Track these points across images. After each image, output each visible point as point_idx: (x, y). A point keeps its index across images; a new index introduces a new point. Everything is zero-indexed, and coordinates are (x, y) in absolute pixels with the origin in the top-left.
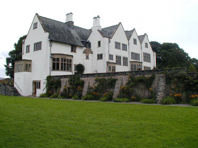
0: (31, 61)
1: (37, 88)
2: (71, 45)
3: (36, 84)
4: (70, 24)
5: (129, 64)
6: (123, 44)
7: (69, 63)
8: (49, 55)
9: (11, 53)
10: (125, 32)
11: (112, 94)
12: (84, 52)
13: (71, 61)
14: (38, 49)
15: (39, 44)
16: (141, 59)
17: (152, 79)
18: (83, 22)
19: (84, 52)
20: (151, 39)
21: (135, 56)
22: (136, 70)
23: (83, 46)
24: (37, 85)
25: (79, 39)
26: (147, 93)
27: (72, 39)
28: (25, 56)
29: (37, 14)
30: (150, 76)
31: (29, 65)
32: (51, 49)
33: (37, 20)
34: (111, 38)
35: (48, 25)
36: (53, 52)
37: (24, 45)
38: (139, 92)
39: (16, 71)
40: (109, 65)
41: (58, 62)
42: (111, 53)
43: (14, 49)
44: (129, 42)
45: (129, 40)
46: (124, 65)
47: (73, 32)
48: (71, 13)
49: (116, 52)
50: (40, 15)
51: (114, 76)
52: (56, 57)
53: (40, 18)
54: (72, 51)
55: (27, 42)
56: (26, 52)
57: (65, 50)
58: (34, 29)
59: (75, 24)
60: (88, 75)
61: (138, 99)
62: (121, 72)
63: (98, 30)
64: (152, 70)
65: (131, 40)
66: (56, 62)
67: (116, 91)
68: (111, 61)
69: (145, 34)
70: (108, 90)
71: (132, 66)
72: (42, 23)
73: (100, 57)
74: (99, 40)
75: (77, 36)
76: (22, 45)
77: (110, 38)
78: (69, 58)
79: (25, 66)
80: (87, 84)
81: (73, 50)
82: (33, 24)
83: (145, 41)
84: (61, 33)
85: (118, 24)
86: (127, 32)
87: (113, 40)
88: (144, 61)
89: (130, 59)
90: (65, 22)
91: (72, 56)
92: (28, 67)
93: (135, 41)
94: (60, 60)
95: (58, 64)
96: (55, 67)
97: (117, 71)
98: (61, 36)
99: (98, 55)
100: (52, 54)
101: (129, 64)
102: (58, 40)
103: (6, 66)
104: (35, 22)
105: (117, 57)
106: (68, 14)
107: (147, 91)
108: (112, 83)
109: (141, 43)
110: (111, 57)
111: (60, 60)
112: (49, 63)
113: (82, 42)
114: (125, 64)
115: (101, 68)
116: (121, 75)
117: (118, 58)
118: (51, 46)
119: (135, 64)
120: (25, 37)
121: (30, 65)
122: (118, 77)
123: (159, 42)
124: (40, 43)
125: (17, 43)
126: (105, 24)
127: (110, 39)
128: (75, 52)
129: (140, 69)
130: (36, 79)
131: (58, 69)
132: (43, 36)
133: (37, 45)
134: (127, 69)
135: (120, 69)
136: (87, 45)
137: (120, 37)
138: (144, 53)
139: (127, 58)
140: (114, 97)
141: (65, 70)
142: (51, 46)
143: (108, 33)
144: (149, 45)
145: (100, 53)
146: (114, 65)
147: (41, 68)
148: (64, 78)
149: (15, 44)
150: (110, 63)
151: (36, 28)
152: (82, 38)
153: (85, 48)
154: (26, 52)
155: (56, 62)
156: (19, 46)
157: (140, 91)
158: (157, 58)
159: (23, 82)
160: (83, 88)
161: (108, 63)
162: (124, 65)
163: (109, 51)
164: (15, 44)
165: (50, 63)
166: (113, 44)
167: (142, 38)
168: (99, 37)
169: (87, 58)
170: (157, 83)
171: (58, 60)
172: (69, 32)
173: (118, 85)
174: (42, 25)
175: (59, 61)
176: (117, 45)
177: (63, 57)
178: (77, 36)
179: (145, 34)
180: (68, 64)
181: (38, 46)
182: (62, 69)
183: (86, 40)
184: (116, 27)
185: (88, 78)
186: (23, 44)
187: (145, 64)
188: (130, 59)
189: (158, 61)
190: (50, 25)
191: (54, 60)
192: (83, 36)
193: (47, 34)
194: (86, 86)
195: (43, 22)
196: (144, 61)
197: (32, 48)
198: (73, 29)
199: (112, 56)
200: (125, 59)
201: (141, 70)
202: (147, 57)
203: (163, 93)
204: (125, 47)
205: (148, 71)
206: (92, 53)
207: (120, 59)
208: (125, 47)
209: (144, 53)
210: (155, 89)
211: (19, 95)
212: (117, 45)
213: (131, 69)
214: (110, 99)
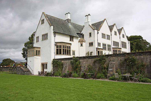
0: (40, 48)
1: (45, 68)
7: (69, 49)
16: (120, 46)
21: (116, 43)
33: (44, 17)
40: (98, 50)
41: (61, 49)
52: (59, 44)
54: (70, 40)
55: (36, 36)
65: (113, 32)
66: (59, 48)
68: (99, 47)
74: (90, 32)
78: (69, 45)
82: (41, 21)
83: (122, 33)
87: (101, 32)
91: (71, 44)
93: (116, 34)
94: (62, 47)
95: (60, 50)
96: (58, 52)
100: (56, 43)
104: (42, 19)
109: (120, 34)
110: (99, 44)
111: (62, 47)
112: (53, 49)
114: (109, 49)
116: (114, 56)
117: (104, 45)
127: (98, 31)
131: (60, 53)
137: (104, 29)
143: (97, 26)
145: (91, 41)
146: (101, 50)
155: (59, 48)
161: (97, 49)
166: (100, 35)
169: (82, 45)
171: (60, 46)
175: (61, 48)
176: (103, 36)
187: (123, 50)
191: (57, 47)
200: (109, 46)
208: (109, 37)
212: (103, 36)
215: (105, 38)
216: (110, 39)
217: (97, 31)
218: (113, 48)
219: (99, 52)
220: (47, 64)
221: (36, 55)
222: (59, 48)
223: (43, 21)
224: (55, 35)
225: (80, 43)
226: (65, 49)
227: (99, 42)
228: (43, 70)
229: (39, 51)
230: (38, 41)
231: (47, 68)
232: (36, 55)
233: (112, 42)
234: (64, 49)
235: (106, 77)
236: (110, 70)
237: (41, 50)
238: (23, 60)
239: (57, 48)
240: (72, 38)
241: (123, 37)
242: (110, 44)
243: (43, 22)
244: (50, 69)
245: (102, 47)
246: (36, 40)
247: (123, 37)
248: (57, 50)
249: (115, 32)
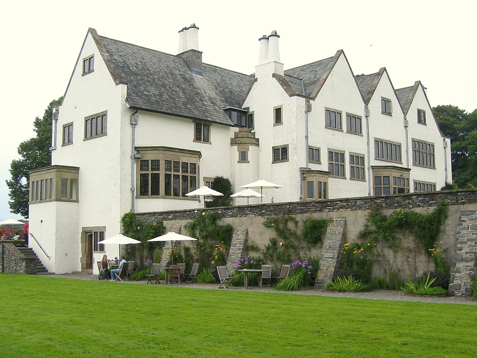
0: (77, 169)
1: (96, 250)
3: (91, 236)
4: (191, 59)
5: (369, 174)
6: (349, 116)
7: (189, 175)
8: (129, 152)
9: (24, 148)
10: (357, 78)
11: (315, 265)
12: (233, 142)
13: (194, 168)
14: (97, 135)
15: (100, 119)
16: (407, 158)
17: (441, 215)
18: (227, 51)
19: (233, 142)
20: (438, 100)
21: (387, 149)
22: (392, 192)
23: (230, 122)
24: (93, 239)
25: (218, 103)
26: (423, 265)
27: (197, 104)
28: (60, 156)
29: (92, 31)
30: (432, 210)
31: (72, 181)
32: (133, 134)
33: (92, 49)
34: (313, 99)
35: (126, 64)
37: (56, 123)
38: (399, 261)
39: (32, 200)
40: (309, 179)
41: (155, 174)
42: (313, 143)
43: (35, 135)
44: (366, 108)
45: (366, 102)
46: (353, 177)
47: (200, 82)
48: (194, 26)
49: (328, 140)
50: (101, 33)
51: (321, 210)
52: (150, 156)
53: (101, 41)
54: (198, 138)
55: (63, 119)
56: (64, 144)
57: (176, 135)
58: (84, 74)
59: (205, 59)
60: (243, 210)
61: (393, 284)
62: (341, 200)
63: (274, 75)
64: (438, 193)
65: (376, 103)
66: (150, 172)
67: (327, 257)
68: (314, 167)
69: (419, 83)
70: (302, 254)
71: (377, 179)
72: (106, 58)
73: (281, 154)
74: (277, 104)
75: (213, 95)
76: (51, 124)
77: (309, 98)
78: (189, 160)
79: (60, 183)
80: (242, 237)
81: (201, 135)
83: (418, 103)
84: (164, 86)
85: (333, 54)
86: (359, 79)
87: (320, 104)
88: (414, 164)
89: (371, 161)
90: (175, 53)
91: (198, 154)
92: (68, 185)
93: (386, 109)
94: (162, 165)
95: (156, 178)
96: (147, 186)
97: (332, 195)
98: (165, 96)
99: (275, 150)
100: (137, 149)
101: (369, 174)
102: (155, 107)
103: (10, 185)
104: (86, 55)
105: (331, 153)
106: (186, 29)
107: (423, 258)
108: (315, 233)
109: (405, 110)
110: (313, 154)
111: (162, 165)
112: (126, 175)
113: (226, 110)
114: (358, 174)
115: (282, 185)
116: (342, 207)
117: (336, 156)
118: (133, 125)
119: (386, 173)
120: (58, 103)
121: (75, 182)
122: (334, 215)
123: (460, 108)
124: (103, 116)
125: (41, 118)
126: (293, 59)
127: (311, 101)
128: (207, 140)
129: (401, 190)
130: (91, 222)
131: (155, 192)
132: (109, 96)
133: (94, 121)
134: (363, 189)
135: (341, 188)
136: (245, 119)
137: (338, 93)
138: (414, 141)
139: (363, 158)
140: (321, 276)
141: (176, 194)
142: (133, 125)
143: (303, 83)
144: (430, 118)
145: (280, 143)
146: (322, 179)
148: (175, 218)
149: (37, 119)
150: (310, 171)
151: (90, 71)
152: (227, 100)
153: (237, 129)
154: (64, 144)
155: (150, 172)
156: (44, 126)
157: (402, 258)
158: (453, 156)
159: (48, 229)
160: (228, 250)
161: (305, 172)
162: (353, 177)
163: (307, 137)
164: (37, 119)
165: (132, 174)
166: (318, 116)
167: (406, 96)
168: (277, 95)
169: (243, 158)
170: (452, 233)
171: (156, 164)
172: (189, 81)
173: (332, 239)
174: (108, 62)
175: (158, 169)
176: (333, 119)
177: (170, 156)
178: (213, 95)
179: (419, 83)
180: (185, 178)
181: (96, 126)
182: (167, 193)
183: (240, 105)
184: (327, 65)
185: (244, 219)
186: (54, 121)
187: (418, 174)
188: (371, 161)
189: (459, 164)
190: (131, 62)
191: (143, 164)
192: (231, 92)
193: (123, 89)
194: (237, 240)
195: (111, 55)
196: (414, 164)
197: (78, 131)
198: (200, 74)
199: (318, 150)
200: (358, 160)
201: (406, 191)
202: (424, 154)
203: (472, 264)
204: (355, 125)
205: (427, 194)
206: (258, 145)
207: (343, 160)
208: (355, 125)
209: (414, 141)
210: (445, 251)
211: (43, 270)
212: (333, 119)
214: (309, 281)
216: (360, 133)
217: (303, 100)
219: (310, 184)
222: (152, 169)
223: (89, 60)
224: (136, 121)
226: (173, 173)
227: (312, 143)
230: (70, 142)
234: (191, 172)
238: (15, 219)
241: (421, 118)
243: (88, 66)
245: (324, 166)
247: (420, 121)
248: (143, 179)
249: (386, 102)
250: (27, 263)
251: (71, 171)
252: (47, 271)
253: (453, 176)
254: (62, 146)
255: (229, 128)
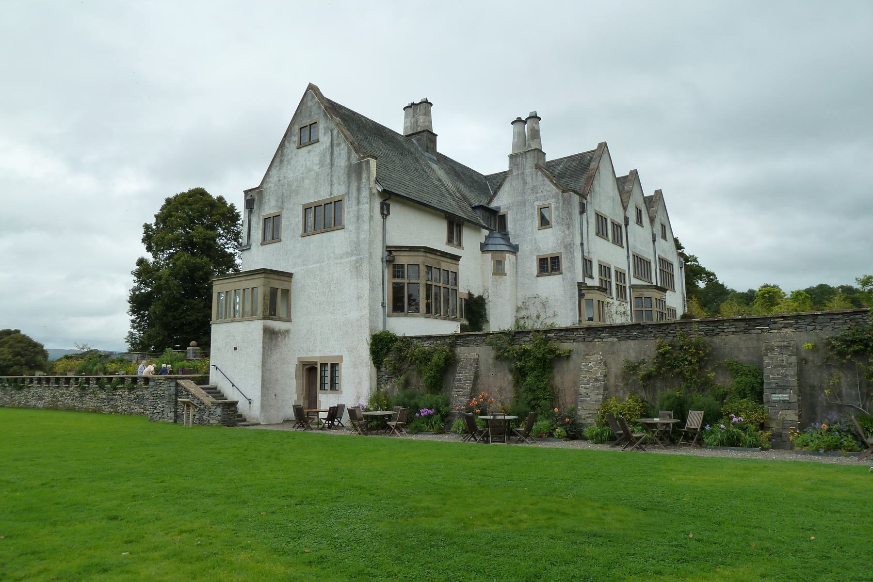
0: (290, 275)
1: (322, 388)
2: (446, 218)
8: (379, 253)
18: (475, 142)
24: (317, 375)
32: (384, 229)
36: (395, 240)
41: (408, 283)
54: (450, 241)
56: (264, 242)
73: (549, 265)
82: (296, 128)
91: (457, 258)
96: (400, 302)
106: (413, 104)
128: (460, 245)
136: (496, 221)
147: (338, 308)
154: (264, 242)
161: (582, 288)
169: (499, 269)
175: (403, 277)
191: (398, 271)
213: (639, 313)
215: (607, 239)
218: (633, 287)
220: (334, 366)
221: (271, 314)
222: (403, 277)
225: (493, 258)
228: (312, 400)
229: (286, 293)
231: (333, 387)
232: (271, 314)
233: (628, 257)
235: (442, 421)
236: (775, 397)
237: (296, 286)
239: (394, 277)
240: (455, 226)
242: (623, 266)
244: (356, 387)
246: (260, 232)
248: (398, 290)
249: (639, 212)
250: (223, 410)
251: (283, 278)
252: (245, 420)
253: (446, 317)
254: (262, 244)
255: (480, 231)
